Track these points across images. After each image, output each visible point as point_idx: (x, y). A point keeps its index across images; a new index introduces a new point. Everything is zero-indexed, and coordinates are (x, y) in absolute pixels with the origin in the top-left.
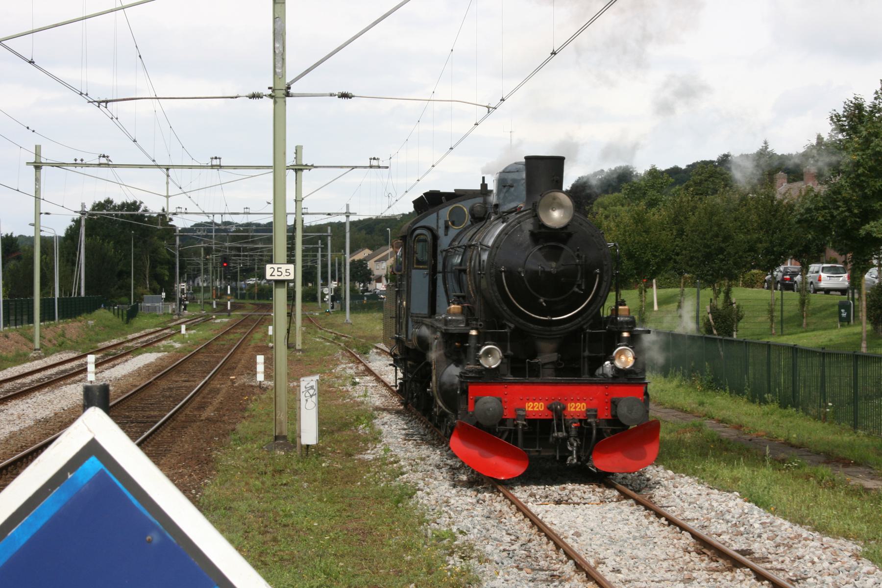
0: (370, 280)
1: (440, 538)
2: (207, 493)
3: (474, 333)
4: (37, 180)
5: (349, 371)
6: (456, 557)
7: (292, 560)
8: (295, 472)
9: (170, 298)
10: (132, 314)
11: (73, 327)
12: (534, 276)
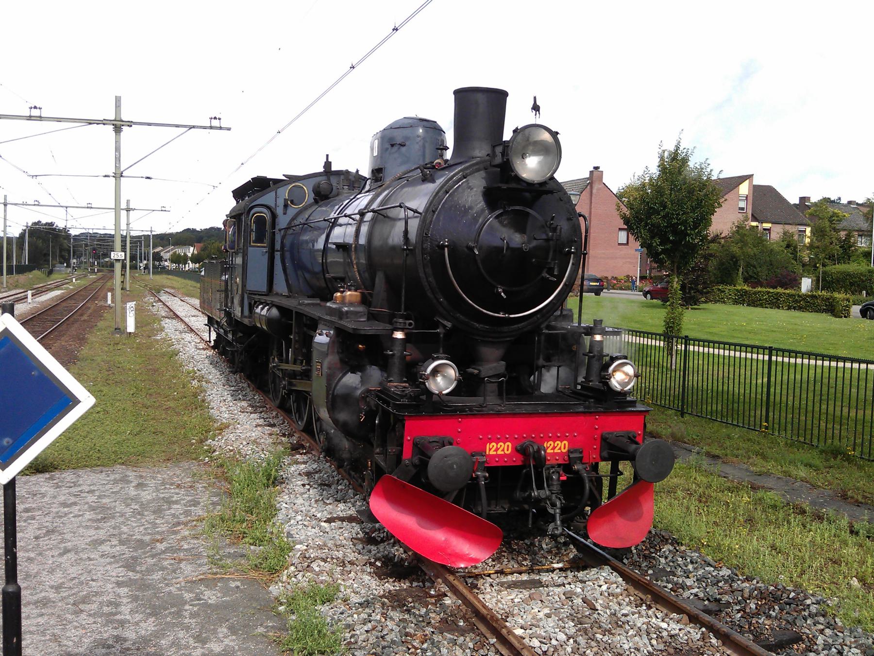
0: (162, 261)
1: (189, 373)
2: (82, 353)
3: (399, 335)
4: (5, 211)
5: (151, 300)
6: (196, 381)
7: (121, 382)
8: (124, 344)
9: (68, 266)
10: (50, 272)
11: (22, 278)
12: (494, 253)
